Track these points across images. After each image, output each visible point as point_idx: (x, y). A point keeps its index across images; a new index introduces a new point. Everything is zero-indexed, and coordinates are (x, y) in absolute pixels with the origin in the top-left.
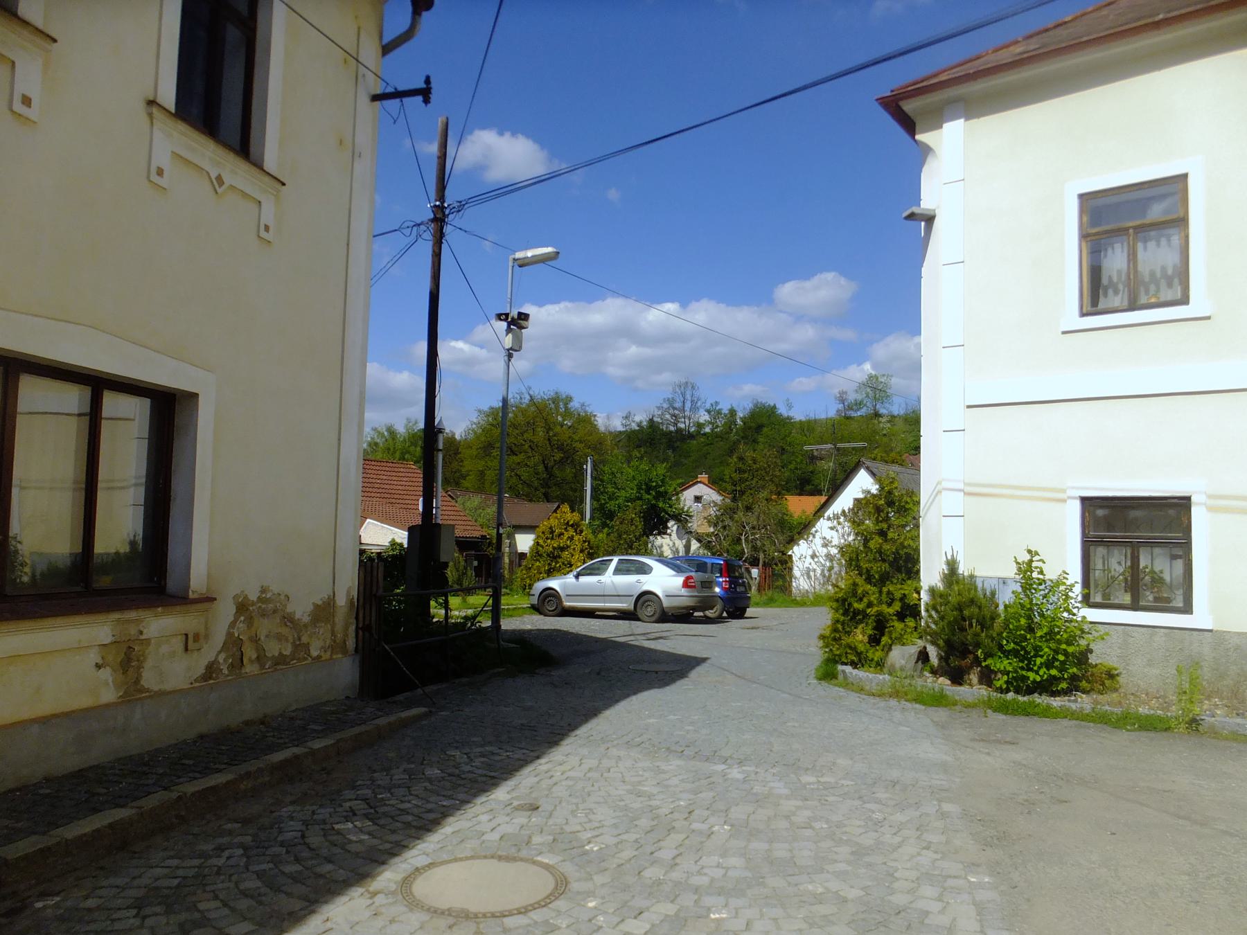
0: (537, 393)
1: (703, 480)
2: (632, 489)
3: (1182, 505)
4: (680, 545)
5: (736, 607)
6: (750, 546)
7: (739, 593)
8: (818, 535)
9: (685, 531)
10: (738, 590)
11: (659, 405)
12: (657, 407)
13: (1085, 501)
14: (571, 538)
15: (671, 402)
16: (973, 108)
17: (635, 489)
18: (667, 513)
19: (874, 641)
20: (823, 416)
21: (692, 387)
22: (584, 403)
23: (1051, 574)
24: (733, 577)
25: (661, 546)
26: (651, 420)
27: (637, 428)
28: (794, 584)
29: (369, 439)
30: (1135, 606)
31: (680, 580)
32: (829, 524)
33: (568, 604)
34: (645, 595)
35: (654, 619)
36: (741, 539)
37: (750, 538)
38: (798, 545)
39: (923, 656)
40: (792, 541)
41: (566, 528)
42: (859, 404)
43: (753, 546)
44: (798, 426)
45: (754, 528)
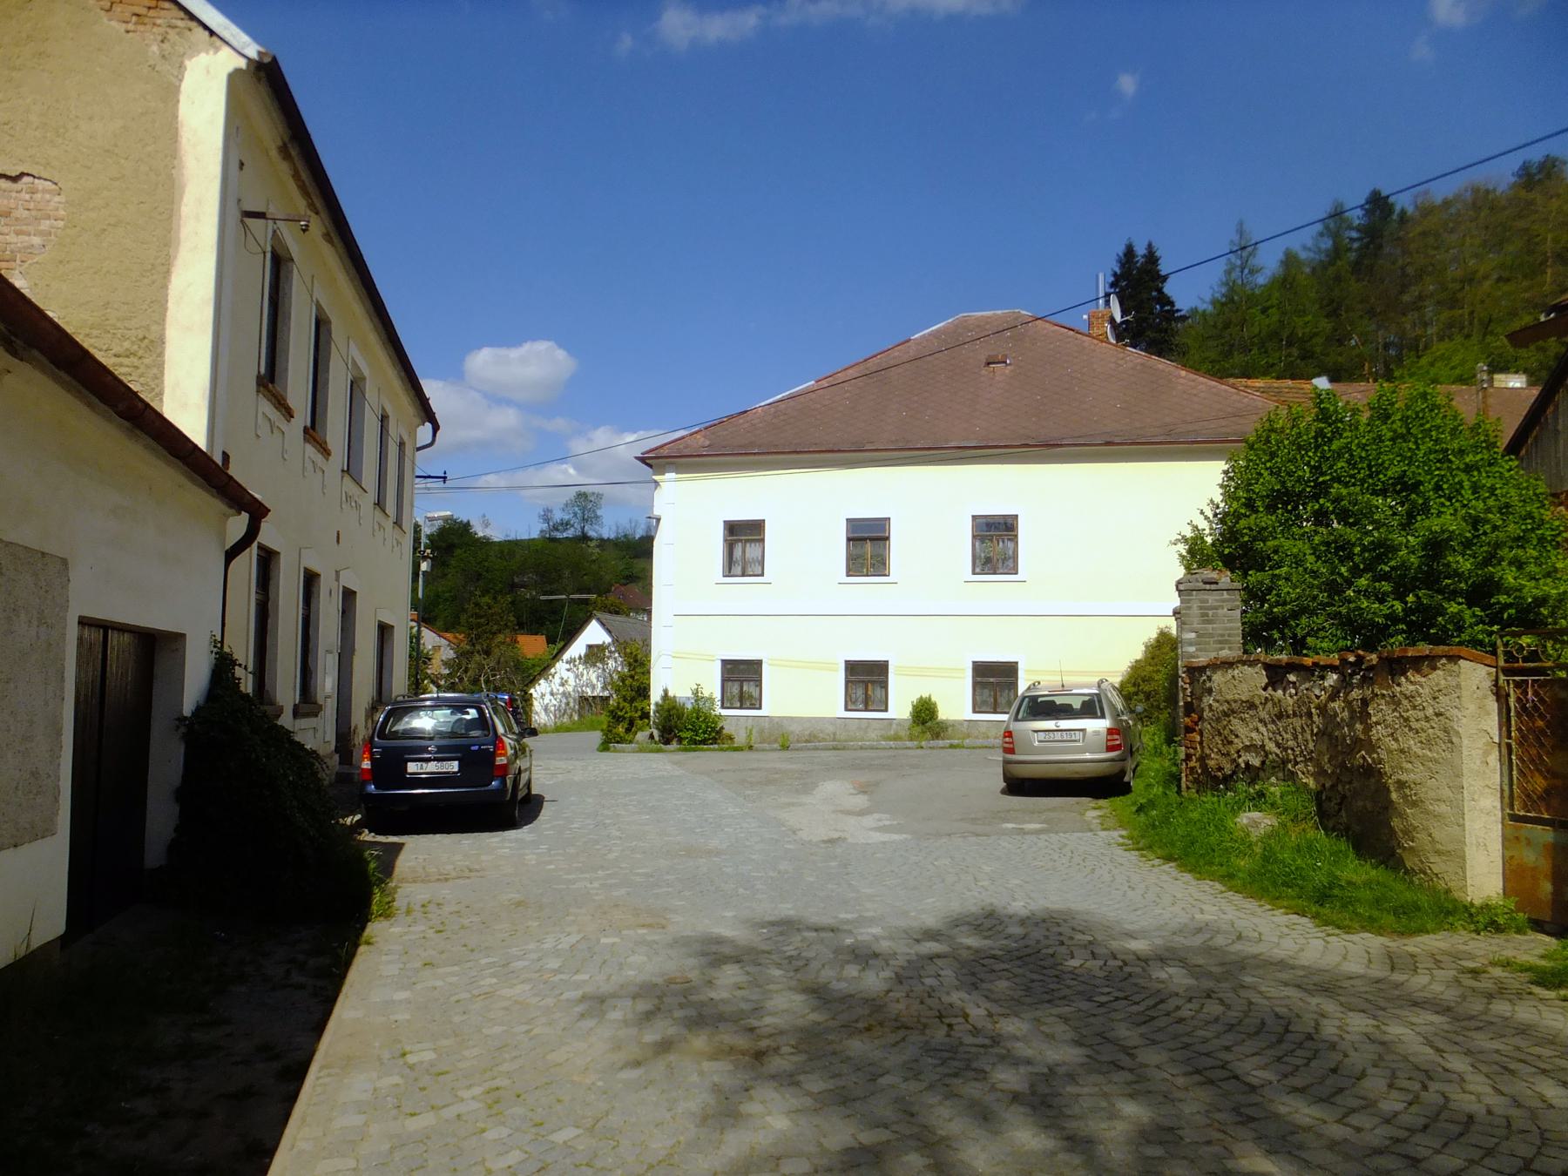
3: (759, 663)
8: (557, 676)
13: (723, 661)
16: (679, 469)
19: (628, 730)
20: (525, 537)
23: (706, 694)
30: (741, 708)
32: (568, 666)
39: (652, 736)
40: (533, 681)
42: (566, 525)
44: (497, 548)
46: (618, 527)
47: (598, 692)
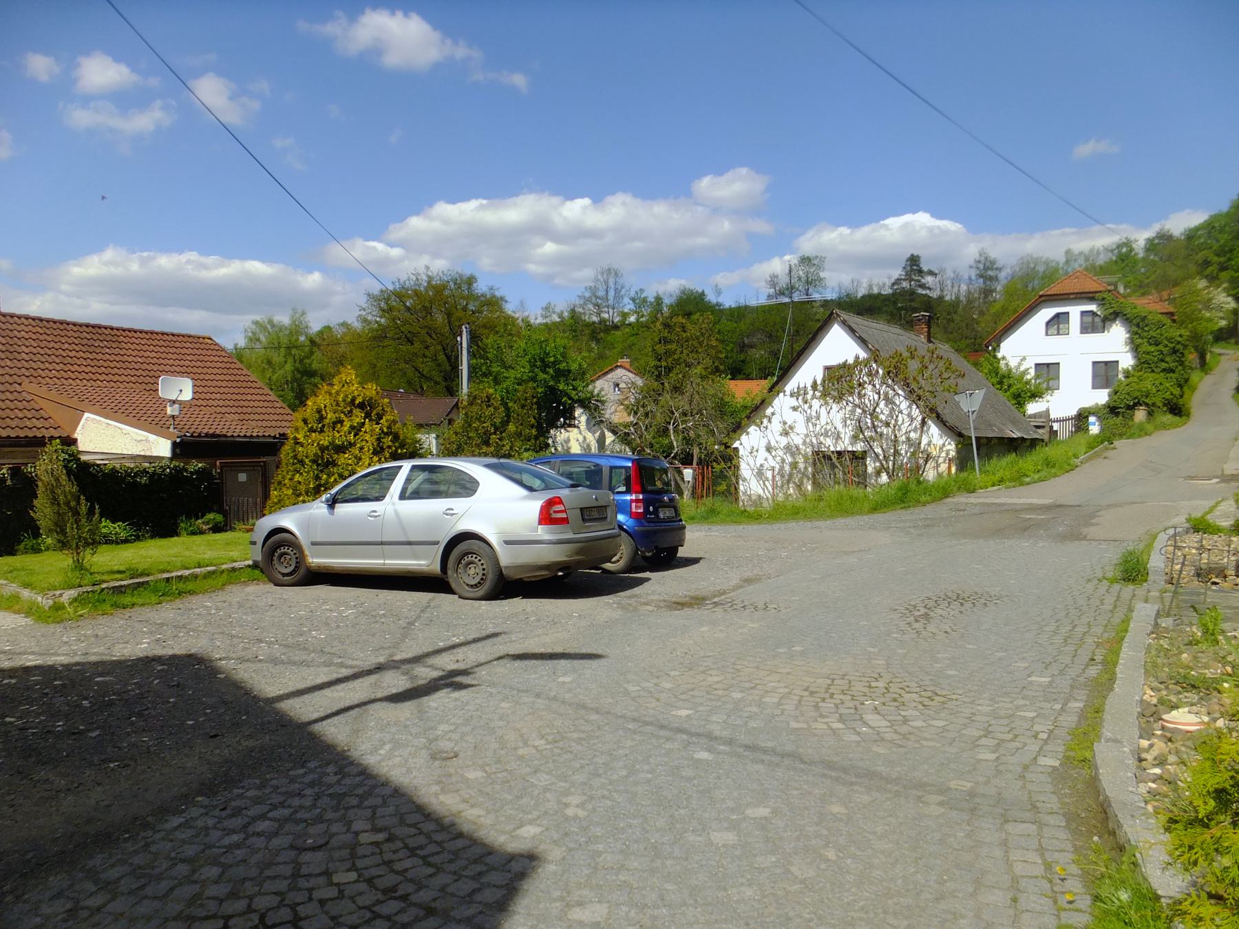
0: (435, 274)
2: (524, 367)
4: (592, 439)
5: (656, 547)
9: (596, 421)
10: (661, 516)
12: (579, 296)
14: (356, 430)
15: (593, 290)
18: (570, 398)
21: (616, 273)
24: (652, 492)
25: (568, 441)
26: (573, 311)
27: (558, 320)
28: (741, 488)
29: (250, 334)
31: (534, 506)
32: (793, 402)
33: (316, 560)
35: (481, 592)
36: (668, 429)
38: (748, 434)
40: (738, 429)
41: (351, 412)
43: (685, 438)
46: (840, 287)
47: (845, 444)
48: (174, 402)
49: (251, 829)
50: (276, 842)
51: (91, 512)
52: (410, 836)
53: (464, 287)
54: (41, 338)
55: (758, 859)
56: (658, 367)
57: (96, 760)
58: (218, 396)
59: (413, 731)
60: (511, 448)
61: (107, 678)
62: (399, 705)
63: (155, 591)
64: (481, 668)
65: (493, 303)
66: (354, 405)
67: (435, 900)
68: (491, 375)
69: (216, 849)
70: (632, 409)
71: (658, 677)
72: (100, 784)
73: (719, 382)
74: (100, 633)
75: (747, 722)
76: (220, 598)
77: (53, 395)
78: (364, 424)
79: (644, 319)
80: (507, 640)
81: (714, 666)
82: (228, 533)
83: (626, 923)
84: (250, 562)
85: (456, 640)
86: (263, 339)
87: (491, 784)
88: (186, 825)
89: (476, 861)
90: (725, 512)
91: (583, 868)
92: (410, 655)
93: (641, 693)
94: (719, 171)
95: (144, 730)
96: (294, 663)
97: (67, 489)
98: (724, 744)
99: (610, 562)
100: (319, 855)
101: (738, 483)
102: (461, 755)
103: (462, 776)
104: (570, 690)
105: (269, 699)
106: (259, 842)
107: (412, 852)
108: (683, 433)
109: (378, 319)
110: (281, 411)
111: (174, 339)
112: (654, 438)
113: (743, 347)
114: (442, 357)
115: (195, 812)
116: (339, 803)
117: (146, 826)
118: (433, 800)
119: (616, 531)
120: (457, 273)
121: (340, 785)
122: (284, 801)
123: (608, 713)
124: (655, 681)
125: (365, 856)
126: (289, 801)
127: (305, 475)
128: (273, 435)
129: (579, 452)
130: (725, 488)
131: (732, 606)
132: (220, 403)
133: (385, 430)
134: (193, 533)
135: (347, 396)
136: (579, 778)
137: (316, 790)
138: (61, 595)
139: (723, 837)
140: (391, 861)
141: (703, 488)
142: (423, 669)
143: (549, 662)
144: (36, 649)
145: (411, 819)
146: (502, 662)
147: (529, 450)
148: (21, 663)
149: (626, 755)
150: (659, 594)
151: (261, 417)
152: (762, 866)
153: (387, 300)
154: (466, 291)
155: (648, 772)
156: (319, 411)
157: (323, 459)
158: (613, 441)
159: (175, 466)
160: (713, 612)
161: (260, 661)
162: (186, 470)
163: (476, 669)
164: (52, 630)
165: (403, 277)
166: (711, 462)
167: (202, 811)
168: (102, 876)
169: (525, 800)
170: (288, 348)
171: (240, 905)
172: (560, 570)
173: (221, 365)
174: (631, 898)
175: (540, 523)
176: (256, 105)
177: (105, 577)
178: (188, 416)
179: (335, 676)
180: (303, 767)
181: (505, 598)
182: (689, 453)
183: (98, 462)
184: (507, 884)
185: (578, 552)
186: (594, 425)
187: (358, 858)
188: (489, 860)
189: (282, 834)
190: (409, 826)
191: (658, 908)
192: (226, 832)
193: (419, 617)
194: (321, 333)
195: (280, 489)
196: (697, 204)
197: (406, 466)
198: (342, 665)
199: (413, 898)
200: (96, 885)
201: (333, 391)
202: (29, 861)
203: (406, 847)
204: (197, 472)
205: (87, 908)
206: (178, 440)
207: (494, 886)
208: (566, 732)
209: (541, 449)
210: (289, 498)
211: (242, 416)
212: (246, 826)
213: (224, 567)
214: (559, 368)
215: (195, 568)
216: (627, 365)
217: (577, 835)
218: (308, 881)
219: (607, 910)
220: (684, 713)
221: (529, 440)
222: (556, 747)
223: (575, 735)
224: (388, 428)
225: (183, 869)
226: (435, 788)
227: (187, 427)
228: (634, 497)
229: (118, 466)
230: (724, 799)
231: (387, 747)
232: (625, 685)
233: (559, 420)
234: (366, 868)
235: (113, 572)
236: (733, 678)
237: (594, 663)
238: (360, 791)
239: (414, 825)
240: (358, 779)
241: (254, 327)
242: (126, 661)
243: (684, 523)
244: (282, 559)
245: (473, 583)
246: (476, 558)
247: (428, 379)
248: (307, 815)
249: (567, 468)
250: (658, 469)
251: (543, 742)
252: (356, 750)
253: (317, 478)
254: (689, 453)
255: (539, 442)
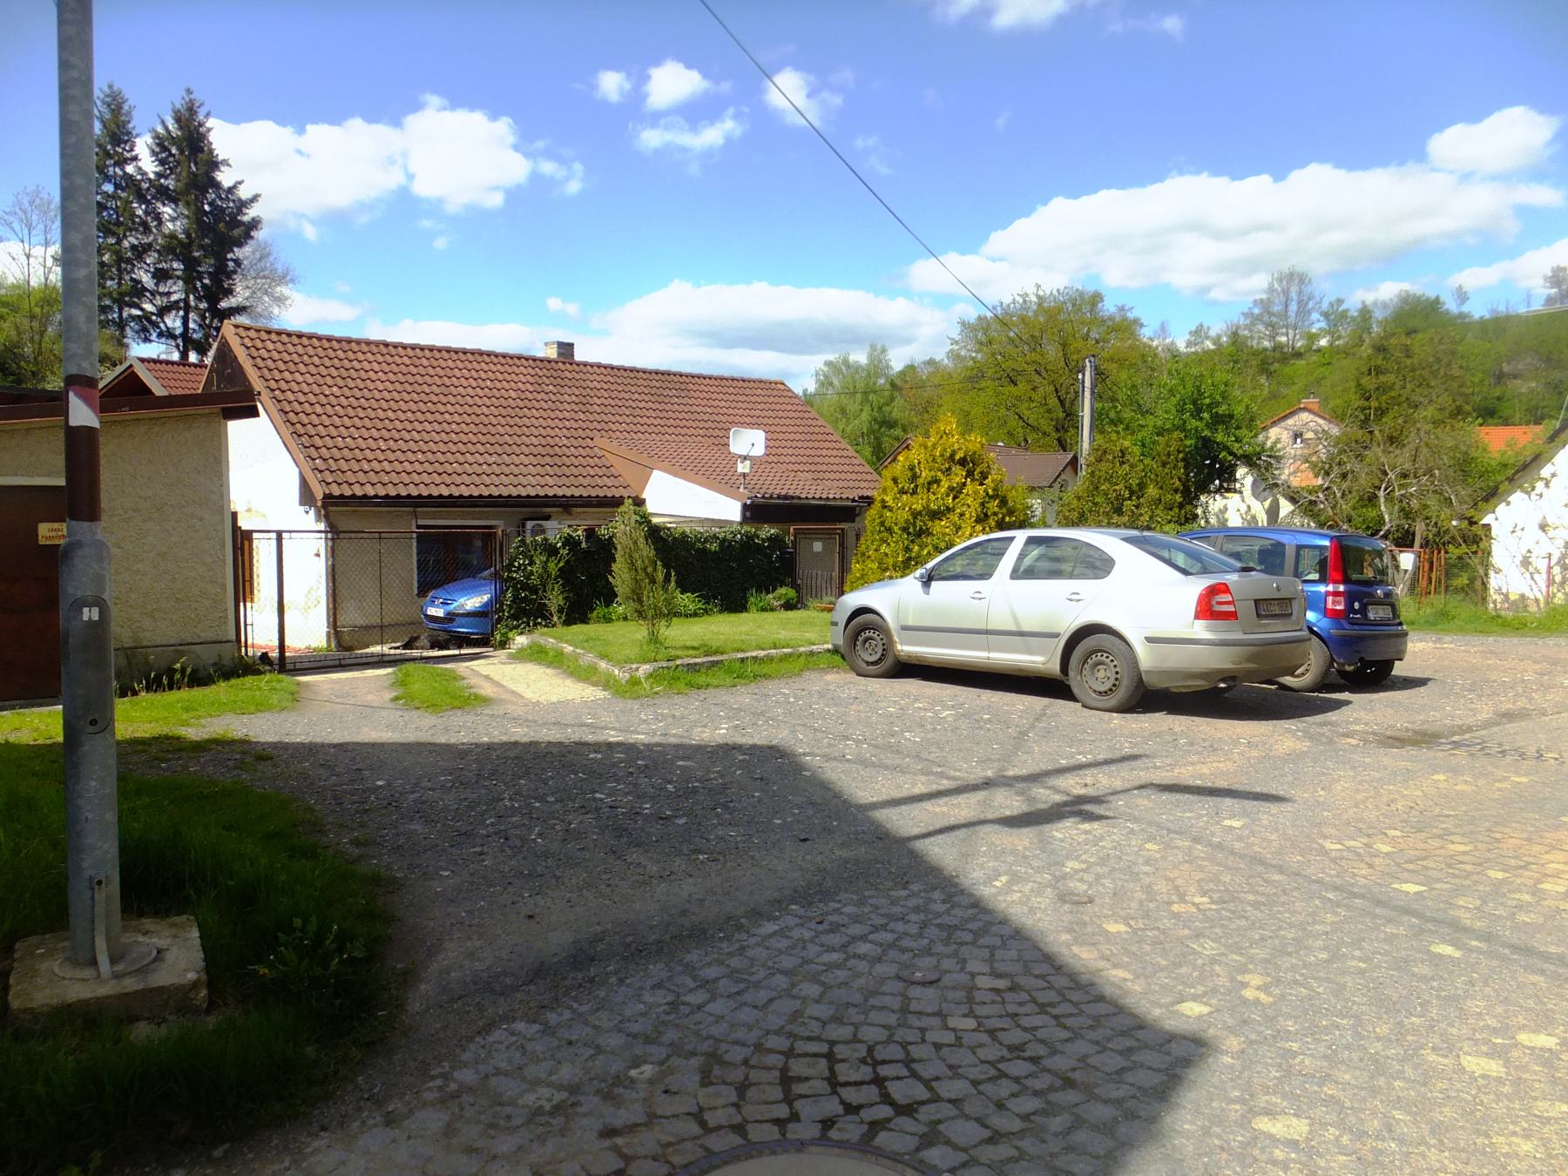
0: (1048, 293)
1: (1311, 406)
4: (1260, 511)
5: (1361, 660)
6: (1396, 507)
7: (1375, 624)
9: (1267, 485)
10: (1371, 616)
11: (1246, 310)
15: (1265, 305)
17: (1174, 411)
18: (1231, 453)
22: (1123, 307)
26: (1235, 335)
29: (822, 377)
33: (907, 648)
34: (1108, 633)
35: (1113, 701)
36: (1376, 496)
37: (1397, 494)
40: (1492, 495)
41: (949, 469)
43: (1403, 509)
45: (1405, 476)
48: (745, 458)
49: (850, 949)
50: (880, 969)
51: (667, 579)
52: (1038, 989)
53: (1086, 308)
54: (613, 387)
55: (1539, 1104)
56: (1365, 409)
57: (685, 851)
58: (790, 451)
59: (1035, 864)
60: (1151, 518)
61: (689, 763)
62: (1015, 831)
63: (730, 671)
64: (1116, 797)
65: (1125, 327)
66: (953, 461)
67: (1074, 1070)
68: (1122, 423)
69: (815, 966)
70: (1323, 468)
71: (1369, 836)
72: (691, 876)
73: (1461, 429)
74: (677, 714)
75: (1514, 914)
76: (797, 686)
77: (623, 451)
78: (964, 484)
79: (1341, 342)
80: (1150, 765)
81: (1458, 830)
82: (800, 612)
83: (1336, 1150)
84: (830, 646)
85: (1082, 759)
86: (836, 382)
87: (1137, 942)
88: (781, 933)
89: (1124, 1033)
90: (1463, 616)
91: (1271, 1069)
92: (1024, 772)
93: (1345, 854)
94: (1475, 114)
95: (730, 824)
96: (887, 768)
97: (645, 554)
98: (1477, 939)
99: (1292, 675)
100: (930, 992)
101: (1486, 575)
102: (1098, 901)
103: (1100, 926)
104: (1240, 839)
105: (861, 805)
106: (862, 966)
107: (1043, 1008)
108: (1401, 501)
109: (974, 354)
110: (860, 469)
111: (745, 386)
112: (1354, 508)
113: (1500, 377)
114: (1053, 401)
115: (791, 921)
116: (950, 935)
117: (740, 928)
118: (1064, 951)
119: (1306, 633)
120: (1077, 290)
121: (949, 915)
122: (887, 924)
123: (1299, 874)
124: (1365, 840)
125: (985, 1003)
126: (892, 925)
127: (893, 545)
128: (851, 497)
129: (1240, 525)
130: (1467, 582)
131: (1482, 749)
132: (793, 459)
133: (990, 492)
134: (763, 610)
135: (945, 450)
136: (1260, 953)
137: (922, 917)
138: (637, 669)
139: (1476, 1064)
140: (1016, 1015)
141: (1433, 577)
142: (1041, 790)
143: (1209, 798)
144: (617, 725)
145: (1039, 969)
146: (1144, 792)
147: (1170, 522)
148: (604, 738)
149: (1327, 933)
150: (1366, 724)
151: (837, 476)
152: (1546, 1115)
153: (986, 330)
154: (1088, 315)
155: (1361, 959)
156: (912, 468)
157: (915, 526)
158: (1294, 511)
159: (747, 532)
160: (1451, 755)
161: (848, 760)
162: (758, 537)
163: (1110, 798)
164: (629, 706)
165: (1007, 300)
166: (1444, 544)
167: (798, 921)
168: (701, 973)
169: (1184, 970)
170: (865, 393)
171: (845, 1032)
172: (1223, 680)
173: (793, 414)
174: (1343, 1119)
175: (1197, 617)
176: (837, 100)
177: (679, 653)
178: (759, 474)
179: (935, 787)
180: (905, 888)
181: (1144, 712)
182: (1407, 531)
183: (669, 525)
184: (1167, 1069)
185: (1249, 659)
186: (1265, 490)
187: (977, 1004)
188: (1140, 1034)
189: (886, 961)
190: (1037, 977)
191: (1384, 1140)
192: (826, 948)
193: (1033, 726)
194: (903, 373)
195: (864, 562)
196: (1433, 170)
197: (1021, 536)
198: (942, 775)
199: (1047, 1063)
200: (695, 981)
201: (930, 444)
202: (629, 945)
203: (1034, 1001)
204: (769, 539)
205: (689, 1004)
206: (749, 502)
207: (1150, 1068)
208: (1237, 892)
209: (1187, 520)
210: (873, 573)
211: (816, 475)
212: (844, 946)
213: (802, 649)
214: (1217, 413)
215: (771, 648)
216: (1315, 408)
217: (1261, 1025)
218: (919, 1020)
219: (1308, 1128)
220: (1411, 888)
221: (1171, 509)
222: (1224, 909)
223: (1251, 897)
224: (994, 490)
225: (781, 981)
226: (1065, 937)
227: (758, 486)
228: (1330, 588)
229: (688, 530)
230: (1481, 1014)
231: (1004, 879)
232: (1320, 841)
233: (1213, 482)
234: (987, 1018)
235: (687, 648)
236: (1489, 850)
237: (1274, 808)
238: (973, 926)
239: (1042, 977)
240: (970, 911)
241: (826, 369)
242: (706, 746)
243: (1405, 627)
244: (867, 645)
245: (1103, 689)
246: (1107, 657)
247: (1035, 429)
248: (912, 944)
249: (1230, 547)
250: (1368, 551)
251: (1205, 899)
252: (966, 878)
253: (907, 549)
254: (1407, 531)
255: (1184, 512)
